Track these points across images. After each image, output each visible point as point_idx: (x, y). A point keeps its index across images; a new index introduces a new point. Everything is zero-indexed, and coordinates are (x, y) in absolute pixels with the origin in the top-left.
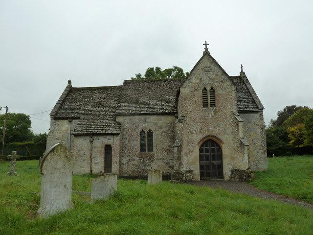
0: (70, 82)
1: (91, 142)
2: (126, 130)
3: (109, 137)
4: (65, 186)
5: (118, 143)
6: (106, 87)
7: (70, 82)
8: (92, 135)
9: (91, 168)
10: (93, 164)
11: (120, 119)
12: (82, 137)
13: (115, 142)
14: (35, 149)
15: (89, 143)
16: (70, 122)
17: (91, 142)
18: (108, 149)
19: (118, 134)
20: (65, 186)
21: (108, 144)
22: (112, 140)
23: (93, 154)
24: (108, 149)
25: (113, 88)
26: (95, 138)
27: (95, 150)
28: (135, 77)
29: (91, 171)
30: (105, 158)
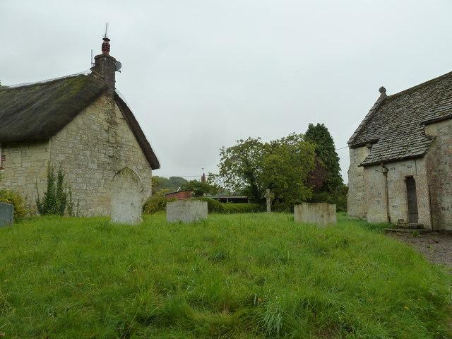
0: (383, 90)
1: (385, 174)
2: (443, 147)
3: (408, 163)
4: (132, 204)
5: (424, 172)
6: (434, 80)
7: (383, 90)
8: (385, 163)
9: (388, 214)
10: (391, 208)
11: (432, 130)
12: (374, 168)
13: (419, 170)
14: (18, 216)
15: (383, 177)
16: (370, 148)
17: (385, 174)
18: (410, 181)
19: (420, 157)
20: (132, 204)
21: (409, 175)
22: (413, 169)
23: (390, 192)
24: (410, 181)
25: (416, 90)
26: (389, 167)
27: (391, 186)
28: (199, 179)
29: (389, 218)
30: (409, 197)
